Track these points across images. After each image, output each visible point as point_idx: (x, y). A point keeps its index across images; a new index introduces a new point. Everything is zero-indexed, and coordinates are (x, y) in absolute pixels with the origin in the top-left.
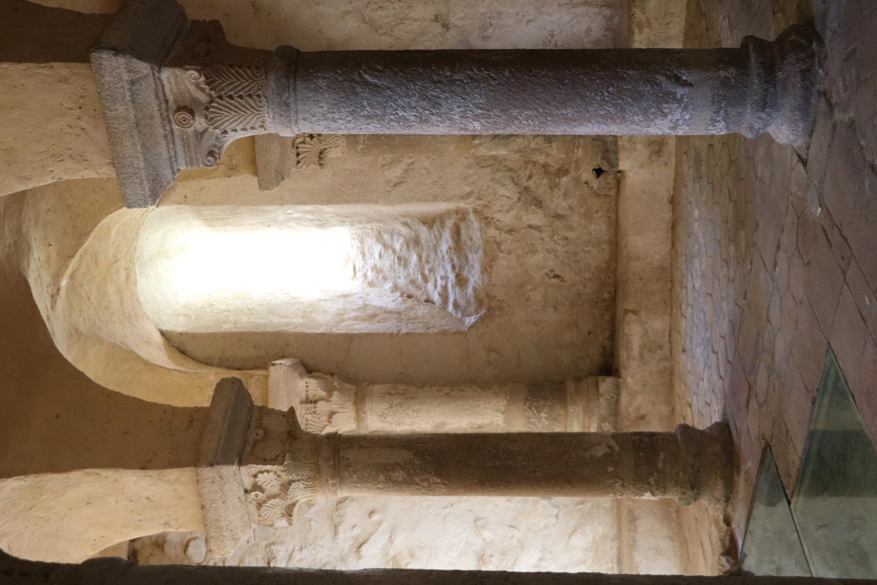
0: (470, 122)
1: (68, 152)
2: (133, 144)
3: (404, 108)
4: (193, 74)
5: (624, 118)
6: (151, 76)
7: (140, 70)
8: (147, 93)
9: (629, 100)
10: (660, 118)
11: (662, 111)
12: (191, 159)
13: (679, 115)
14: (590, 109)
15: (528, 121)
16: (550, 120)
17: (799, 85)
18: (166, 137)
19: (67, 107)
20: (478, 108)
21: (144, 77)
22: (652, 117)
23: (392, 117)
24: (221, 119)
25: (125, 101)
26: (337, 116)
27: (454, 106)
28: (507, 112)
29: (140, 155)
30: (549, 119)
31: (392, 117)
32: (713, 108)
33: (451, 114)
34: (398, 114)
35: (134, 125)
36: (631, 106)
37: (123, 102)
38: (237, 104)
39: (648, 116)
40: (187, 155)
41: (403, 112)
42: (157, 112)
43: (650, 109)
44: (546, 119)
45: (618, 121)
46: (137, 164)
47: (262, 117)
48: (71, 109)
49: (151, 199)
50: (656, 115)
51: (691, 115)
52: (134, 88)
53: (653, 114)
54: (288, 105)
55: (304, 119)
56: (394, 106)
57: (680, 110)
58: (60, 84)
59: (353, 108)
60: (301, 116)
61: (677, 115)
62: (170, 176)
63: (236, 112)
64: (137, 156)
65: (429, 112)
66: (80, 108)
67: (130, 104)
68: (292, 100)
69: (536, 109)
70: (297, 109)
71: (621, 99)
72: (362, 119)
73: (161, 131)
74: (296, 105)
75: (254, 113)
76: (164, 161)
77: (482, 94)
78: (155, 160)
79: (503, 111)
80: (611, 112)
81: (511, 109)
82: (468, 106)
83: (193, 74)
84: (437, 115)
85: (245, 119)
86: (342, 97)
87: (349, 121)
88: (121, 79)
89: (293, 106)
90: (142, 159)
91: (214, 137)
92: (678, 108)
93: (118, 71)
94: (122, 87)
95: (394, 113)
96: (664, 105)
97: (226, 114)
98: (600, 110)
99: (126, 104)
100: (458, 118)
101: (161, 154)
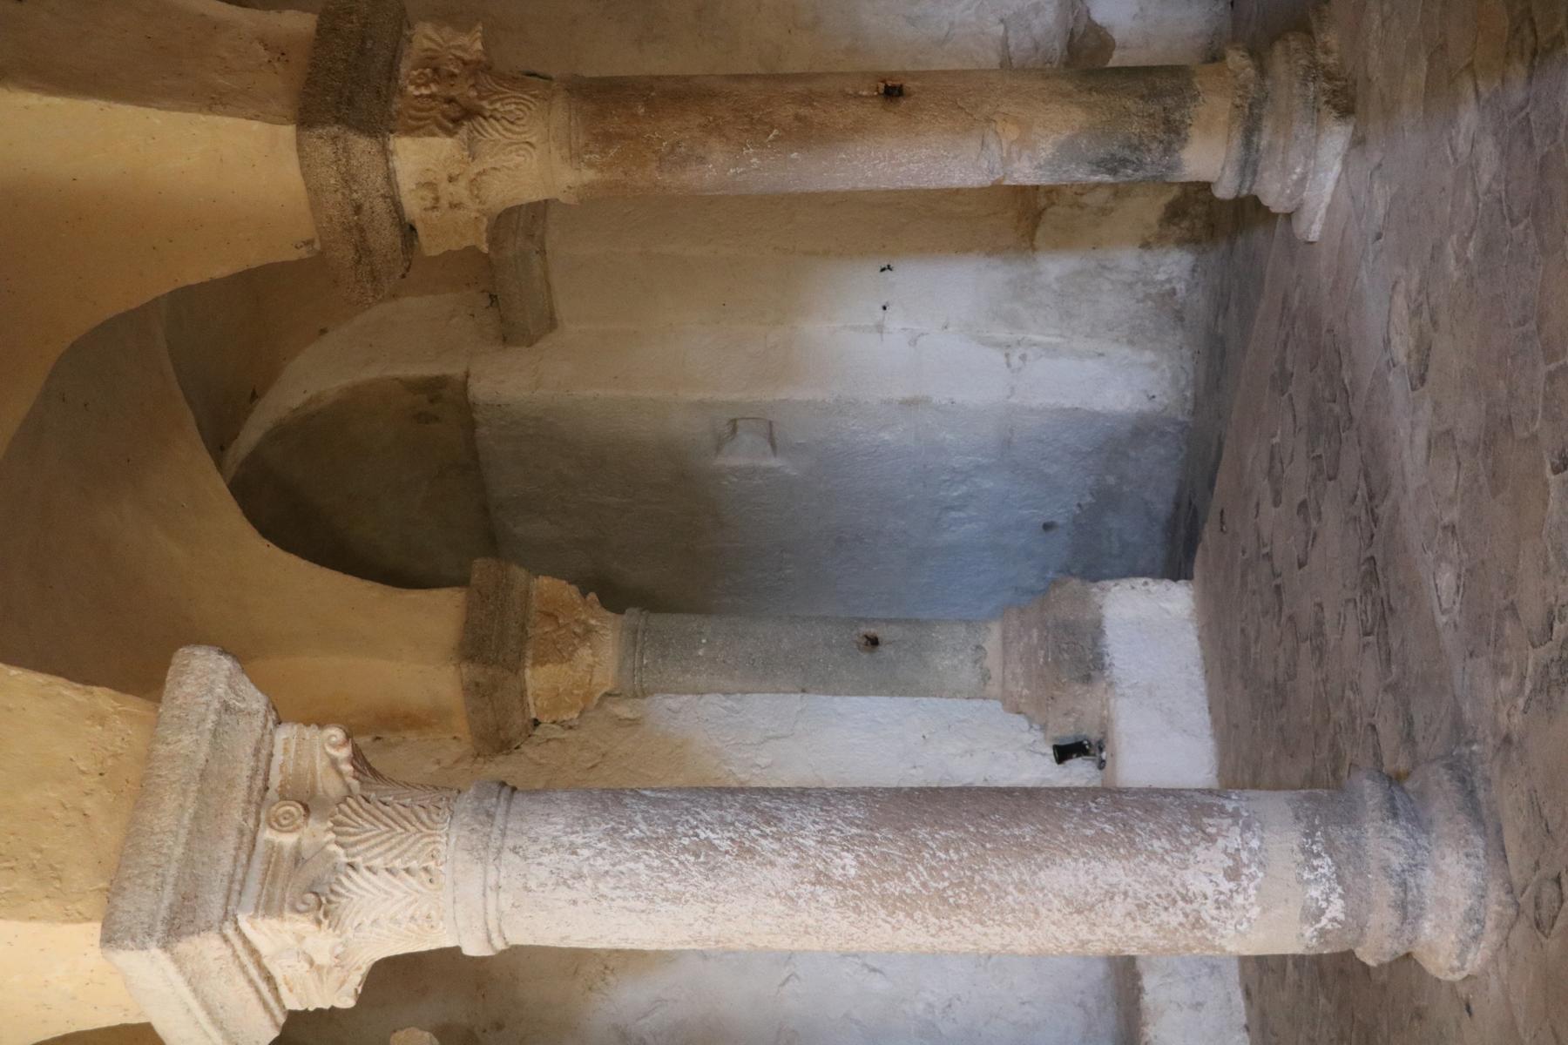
0: (835, 854)
1: (32, 855)
2: (181, 806)
3: (711, 824)
4: (335, 736)
5: (1132, 843)
6: (261, 715)
7: (247, 698)
8: (243, 743)
9: (1137, 811)
10: (1203, 845)
11: (1204, 832)
12: (270, 900)
13: (1239, 840)
14: (1065, 827)
15: (947, 851)
16: (990, 850)
17: (1446, 777)
18: (241, 832)
19: (78, 768)
20: (852, 824)
21: (249, 714)
22: (1187, 842)
23: (686, 841)
24: (355, 834)
25: (200, 728)
26: (578, 840)
27: (807, 822)
28: (906, 833)
29: (183, 832)
30: (988, 846)
31: (686, 841)
32: (1302, 826)
33: (800, 836)
34: (697, 835)
35: (197, 774)
36: (1142, 821)
37: (197, 727)
38: (393, 814)
39: (1177, 840)
40: (265, 892)
41: (708, 831)
42: (245, 779)
43: (1180, 826)
44: (983, 846)
45: (1122, 851)
46: (169, 847)
47: (434, 842)
48: (83, 773)
49: (164, 928)
50: (1193, 838)
51: (1262, 839)
52: (226, 717)
53: (1188, 836)
54: (490, 816)
55: (515, 850)
56: (691, 820)
57: (1237, 830)
58: (88, 722)
59: (613, 824)
60: (510, 843)
61: (1234, 839)
62: (216, 912)
63: (386, 825)
64: (177, 832)
65: (759, 832)
66: (101, 774)
67: (208, 736)
68: (500, 811)
69: (962, 826)
70: (506, 828)
71: (1120, 810)
72: (627, 847)
73: (237, 816)
74: (507, 822)
75: (421, 832)
76: (219, 877)
77: (860, 805)
78: (203, 864)
79: (899, 829)
80: (1107, 831)
81: (915, 827)
82: (834, 822)
83: (335, 736)
84: (772, 837)
85: (400, 843)
86: (596, 809)
87: (601, 852)
88: (211, 691)
89: (499, 820)
90: (184, 840)
91: (329, 865)
92: (1233, 825)
93: (212, 677)
94: (208, 704)
95: (691, 832)
96: (1205, 820)
97: (367, 826)
98: (1085, 827)
99: (200, 733)
100: (813, 844)
101: (219, 860)
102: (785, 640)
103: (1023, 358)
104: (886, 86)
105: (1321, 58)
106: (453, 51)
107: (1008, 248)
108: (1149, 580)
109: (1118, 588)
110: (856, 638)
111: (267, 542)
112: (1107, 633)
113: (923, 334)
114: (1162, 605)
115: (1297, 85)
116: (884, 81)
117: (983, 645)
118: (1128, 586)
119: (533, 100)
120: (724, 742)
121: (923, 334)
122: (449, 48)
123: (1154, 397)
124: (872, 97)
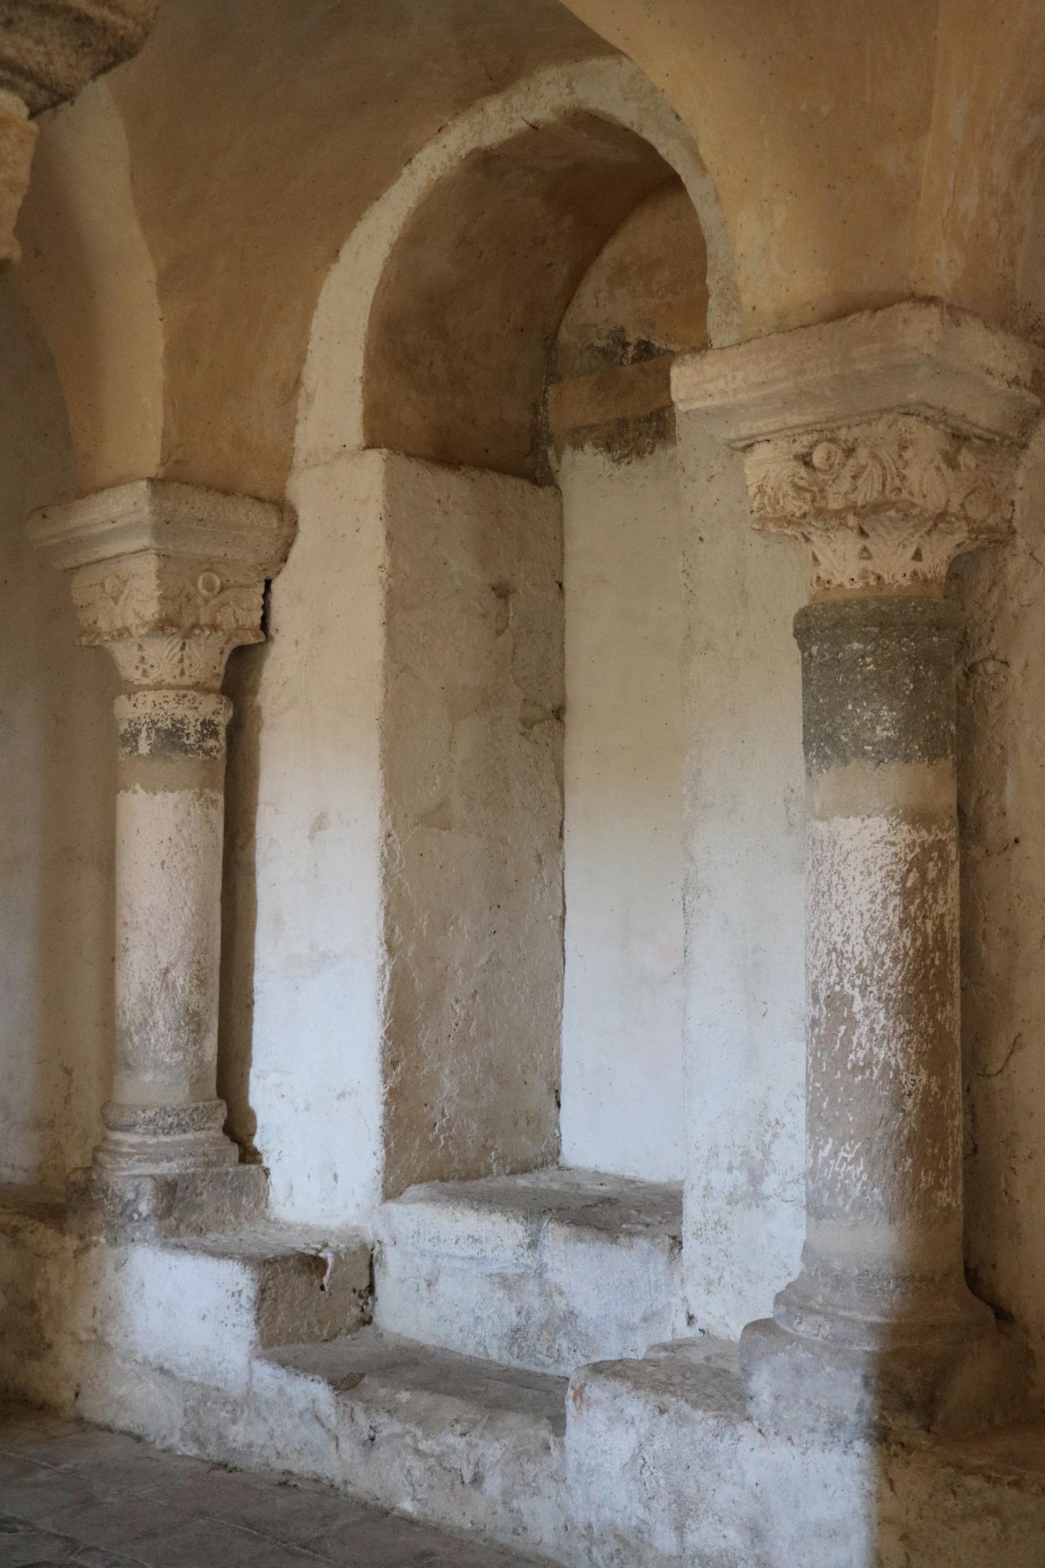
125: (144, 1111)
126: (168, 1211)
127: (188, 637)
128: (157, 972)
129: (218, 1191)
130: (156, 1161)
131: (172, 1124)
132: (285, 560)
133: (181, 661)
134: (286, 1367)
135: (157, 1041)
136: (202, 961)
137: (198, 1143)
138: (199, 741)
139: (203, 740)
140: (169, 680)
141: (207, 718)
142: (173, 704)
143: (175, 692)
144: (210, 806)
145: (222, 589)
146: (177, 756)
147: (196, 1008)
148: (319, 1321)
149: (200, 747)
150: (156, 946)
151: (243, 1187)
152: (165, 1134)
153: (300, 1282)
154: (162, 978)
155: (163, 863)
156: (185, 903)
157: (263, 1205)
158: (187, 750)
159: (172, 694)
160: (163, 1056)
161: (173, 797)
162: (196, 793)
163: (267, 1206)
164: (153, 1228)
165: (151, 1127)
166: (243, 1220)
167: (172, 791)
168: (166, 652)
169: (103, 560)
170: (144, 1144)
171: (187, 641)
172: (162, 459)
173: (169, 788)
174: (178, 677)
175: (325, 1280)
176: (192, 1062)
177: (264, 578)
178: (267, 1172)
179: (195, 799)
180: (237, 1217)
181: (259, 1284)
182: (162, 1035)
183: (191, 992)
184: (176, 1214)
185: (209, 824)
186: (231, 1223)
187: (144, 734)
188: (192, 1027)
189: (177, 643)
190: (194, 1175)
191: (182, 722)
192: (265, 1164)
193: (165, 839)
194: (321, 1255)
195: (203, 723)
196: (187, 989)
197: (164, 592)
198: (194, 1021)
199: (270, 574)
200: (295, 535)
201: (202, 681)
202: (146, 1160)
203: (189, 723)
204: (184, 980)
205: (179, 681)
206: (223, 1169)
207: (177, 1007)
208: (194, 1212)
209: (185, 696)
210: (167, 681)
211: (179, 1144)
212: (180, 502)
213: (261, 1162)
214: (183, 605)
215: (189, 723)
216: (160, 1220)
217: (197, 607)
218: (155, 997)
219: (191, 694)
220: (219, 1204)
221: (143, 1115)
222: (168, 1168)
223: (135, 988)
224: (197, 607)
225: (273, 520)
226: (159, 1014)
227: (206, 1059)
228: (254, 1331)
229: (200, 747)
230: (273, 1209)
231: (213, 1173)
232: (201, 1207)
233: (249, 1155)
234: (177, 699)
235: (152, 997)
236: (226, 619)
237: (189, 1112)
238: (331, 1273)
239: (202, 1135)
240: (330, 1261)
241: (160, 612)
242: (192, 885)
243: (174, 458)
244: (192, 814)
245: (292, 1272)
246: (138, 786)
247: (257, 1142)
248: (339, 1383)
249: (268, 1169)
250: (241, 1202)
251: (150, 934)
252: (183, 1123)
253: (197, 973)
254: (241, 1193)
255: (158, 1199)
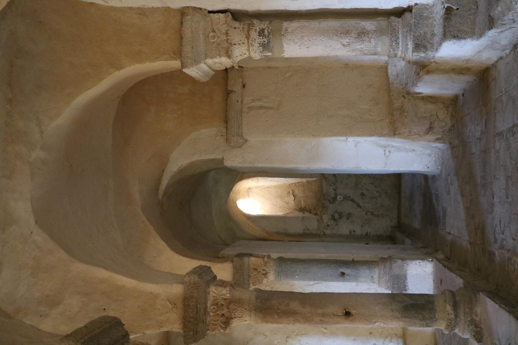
102: (319, 274)
103: (390, 152)
104: (346, 311)
105: (474, 317)
106: (221, 296)
107: (386, 135)
108: (421, 261)
109: (412, 264)
110: (339, 273)
111: (178, 255)
112: (408, 279)
113: (359, 142)
114: (424, 269)
115: (466, 327)
116: (345, 310)
117: (373, 276)
118: (415, 263)
119: (245, 311)
120: (304, 284)
121: (359, 142)
122: (220, 295)
123: (429, 167)
124: (342, 316)
125: (390, 52)
126: (425, 47)
127: (231, 43)
128: (344, 48)
129: (420, 26)
130: (408, 49)
131: (395, 43)
132: (201, 9)
133: (239, 44)
134: (482, 36)
135: (367, 47)
136: (340, 32)
137: (403, 33)
138: (266, 37)
139: (265, 35)
140: (246, 48)
141: (258, 34)
142: (254, 48)
143: (250, 47)
144: (288, 31)
145: (214, 31)
146: (271, 44)
147: (356, 34)
148: (470, 10)
149: (268, 37)
150: (335, 49)
151: (420, 15)
152: (399, 45)
153: (455, 20)
154: (346, 47)
155: (307, 48)
156: (321, 40)
157: (427, 7)
158: (269, 42)
159: (251, 48)
160: (372, 46)
161: (285, 46)
162: (283, 38)
163: (428, 5)
164: (430, 53)
165: (396, 49)
166: (432, 16)
167: (283, 46)
168: (237, 50)
169: (208, 66)
170: (402, 51)
171: (233, 44)
172: (175, 60)
173: (282, 47)
174: (245, 45)
175: (455, 8)
176: (375, 35)
177: (208, 14)
178: (416, 4)
179: (285, 38)
180: (430, 18)
181: (452, 38)
182: (365, 46)
183: (351, 37)
184: (426, 44)
185: (294, 31)
186: (432, 21)
187: (265, 54)
188: (363, 36)
189: (234, 47)
190: (414, 36)
191: (260, 44)
192: (413, 4)
193: (299, 47)
194: (446, 7)
195: (260, 36)
196: (350, 38)
197: (217, 55)
198: (362, 34)
199: (206, 12)
200: (192, 7)
201: (245, 36)
202: (407, 52)
203: (260, 41)
204: (347, 39)
205: (246, 45)
206: (413, 24)
207: (356, 41)
208: (426, 36)
209: (251, 44)
210: (247, 48)
211: (402, 40)
212: (188, 56)
213: (412, 6)
214: (221, 47)
215: (260, 41)
216: (427, 50)
217: (221, 41)
218: (352, 48)
219: (250, 42)
220: (425, 25)
221: (392, 52)
222: (410, 46)
223: (349, 53)
224: (221, 41)
225: (188, 18)
226: (358, 47)
227: (374, 29)
228: (468, 39)
229: (268, 37)
230: (429, 3)
231: (414, 29)
232: (425, 33)
233: (409, 9)
234: (252, 46)
235: (352, 49)
236: (224, 28)
237: (392, 37)
238: (453, 6)
239: (400, 31)
240: (448, 5)
241: (224, 57)
242: (314, 38)
243: (173, 56)
244: (290, 38)
245: (449, 24)
246: (282, 55)
247: (405, 6)
248: (490, 27)
249: (415, 4)
250: (425, 16)
251: (331, 51)
252: (395, 39)
253: (344, 34)
254: (422, 16)
255: (420, 51)
